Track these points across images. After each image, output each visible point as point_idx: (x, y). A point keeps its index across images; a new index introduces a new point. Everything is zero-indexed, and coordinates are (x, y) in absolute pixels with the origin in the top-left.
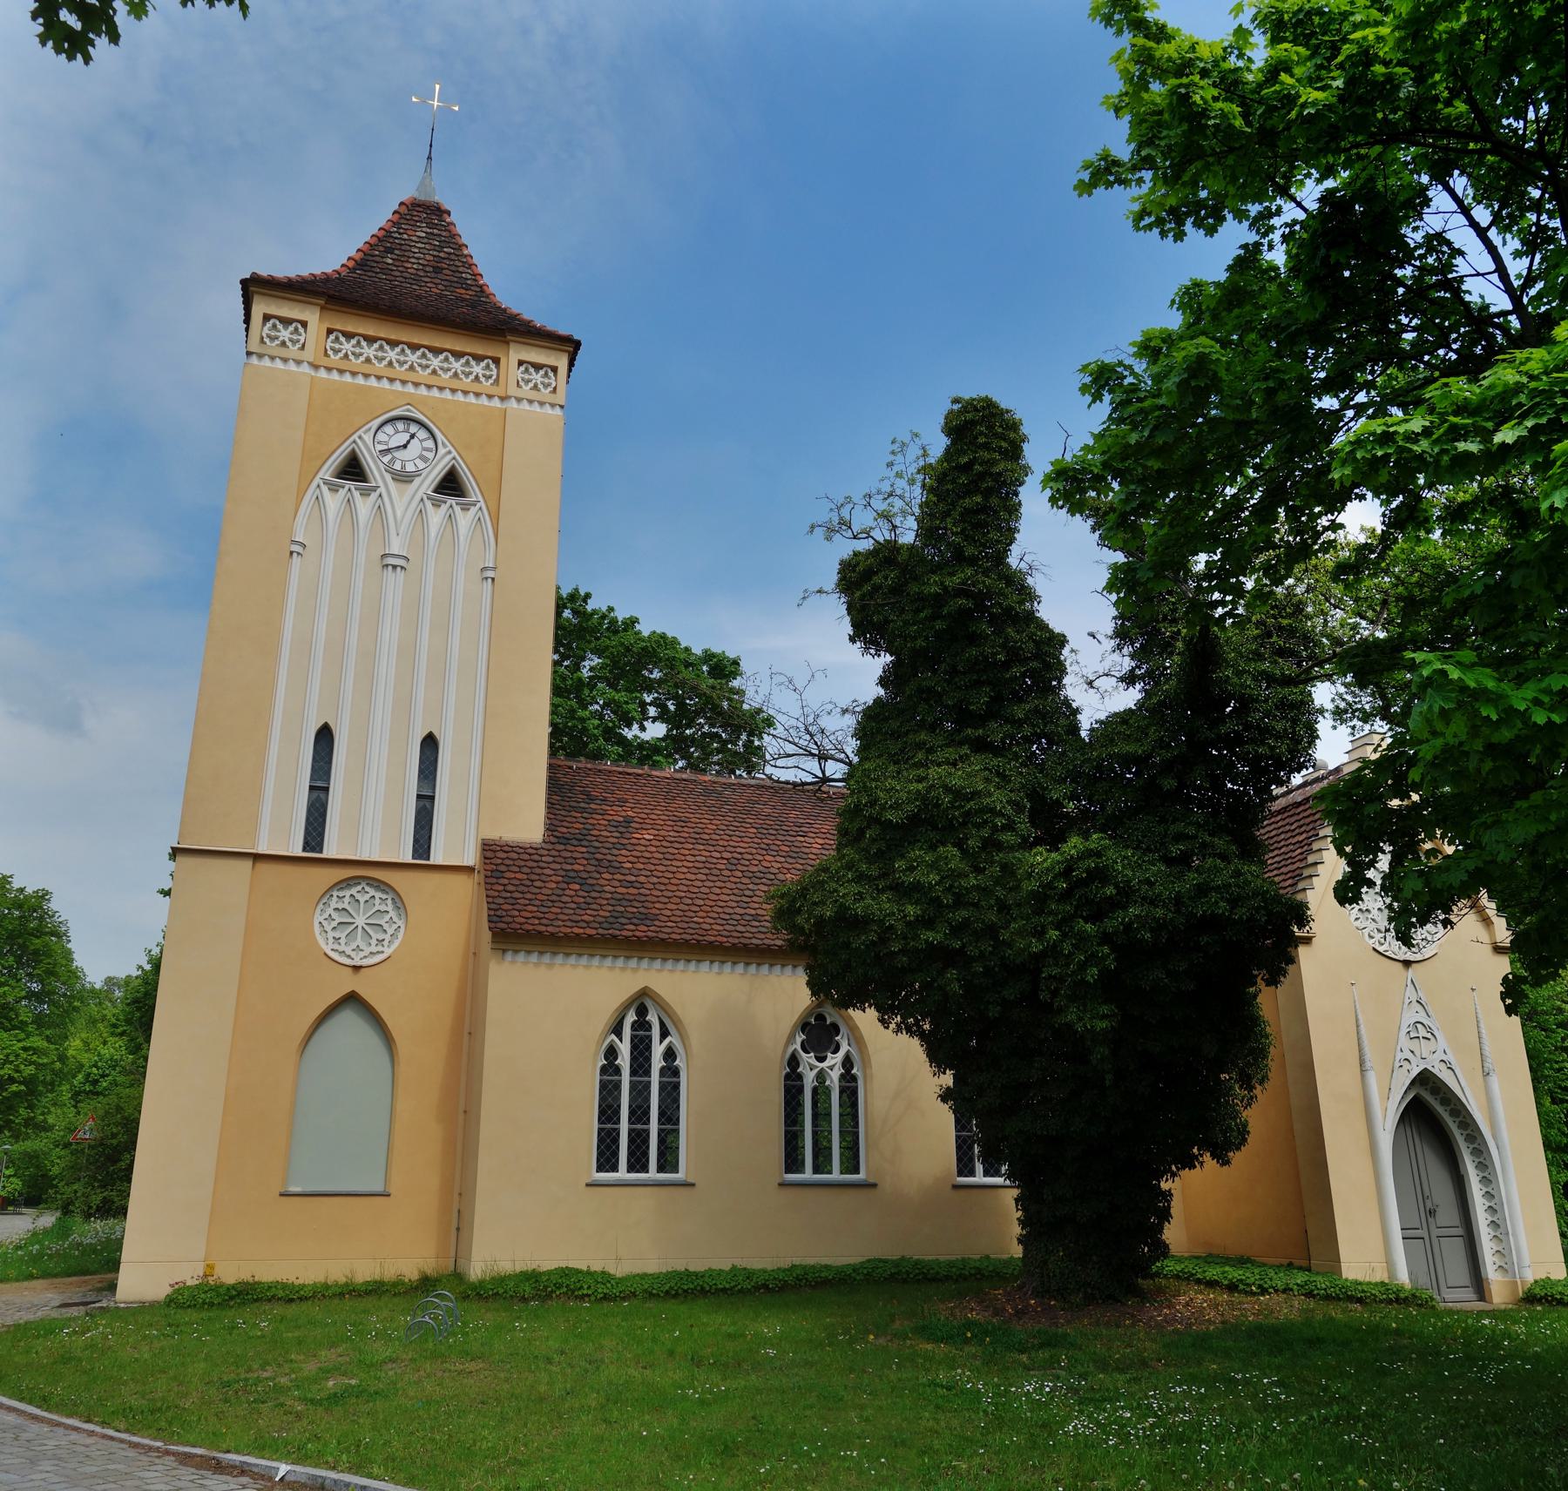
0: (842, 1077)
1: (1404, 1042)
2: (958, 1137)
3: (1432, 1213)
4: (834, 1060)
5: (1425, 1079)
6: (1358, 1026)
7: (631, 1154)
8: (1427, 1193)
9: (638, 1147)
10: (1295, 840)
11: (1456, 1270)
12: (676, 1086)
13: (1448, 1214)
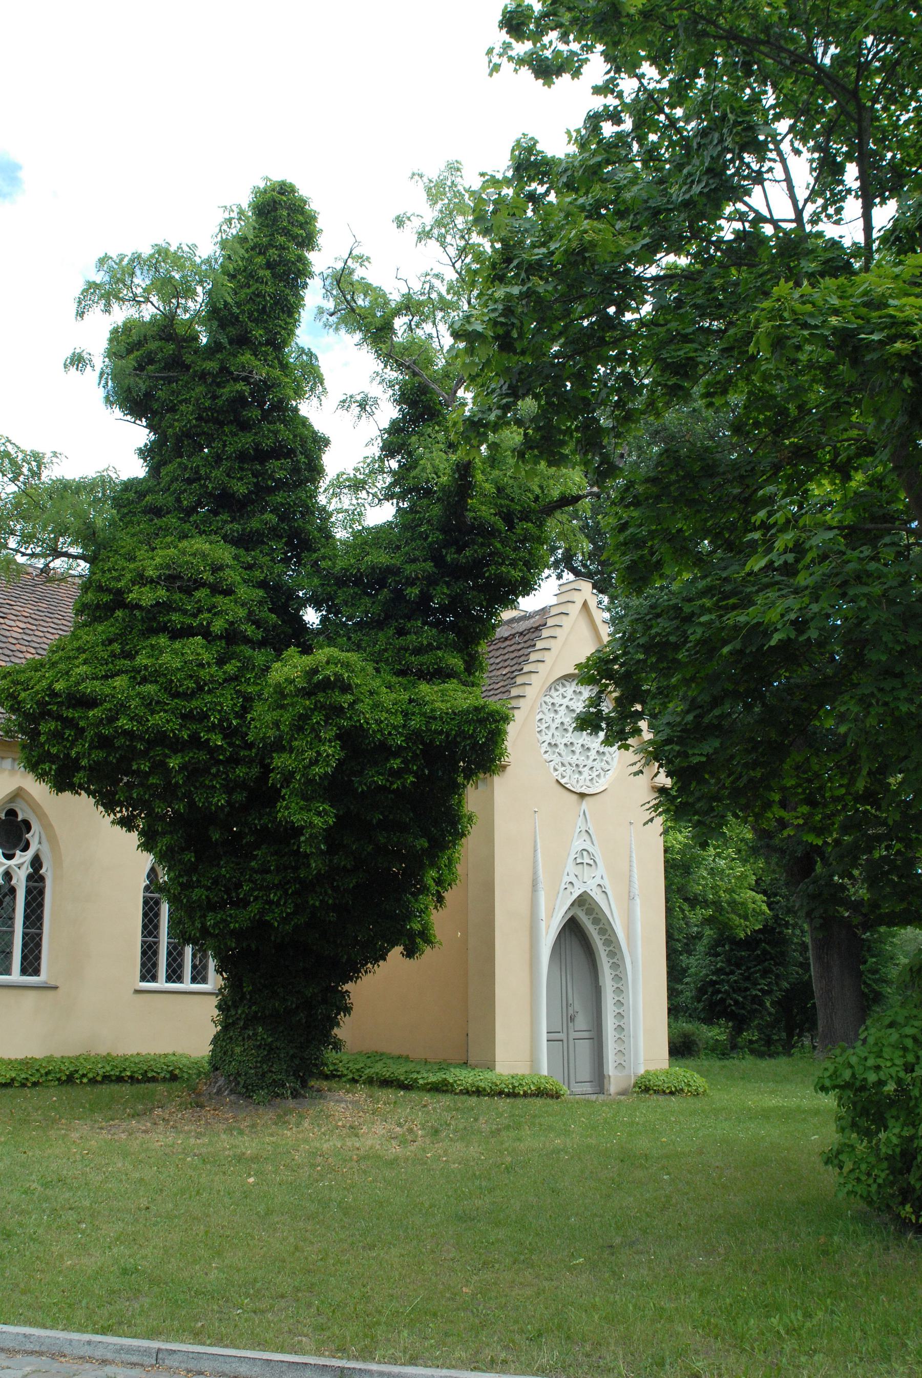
0: (30, 878)
1: (570, 867)
2: (144, 942)
3: (572, 1019)
4: (23, 858)
5: (583, 901)
6: (535, 851)
7: (24, 958)
8: (570, 1002)
9: (149, 959)
10: (499, 673)
11: (584, 1070)
12: (41, 892)
13: (581, 1022)
